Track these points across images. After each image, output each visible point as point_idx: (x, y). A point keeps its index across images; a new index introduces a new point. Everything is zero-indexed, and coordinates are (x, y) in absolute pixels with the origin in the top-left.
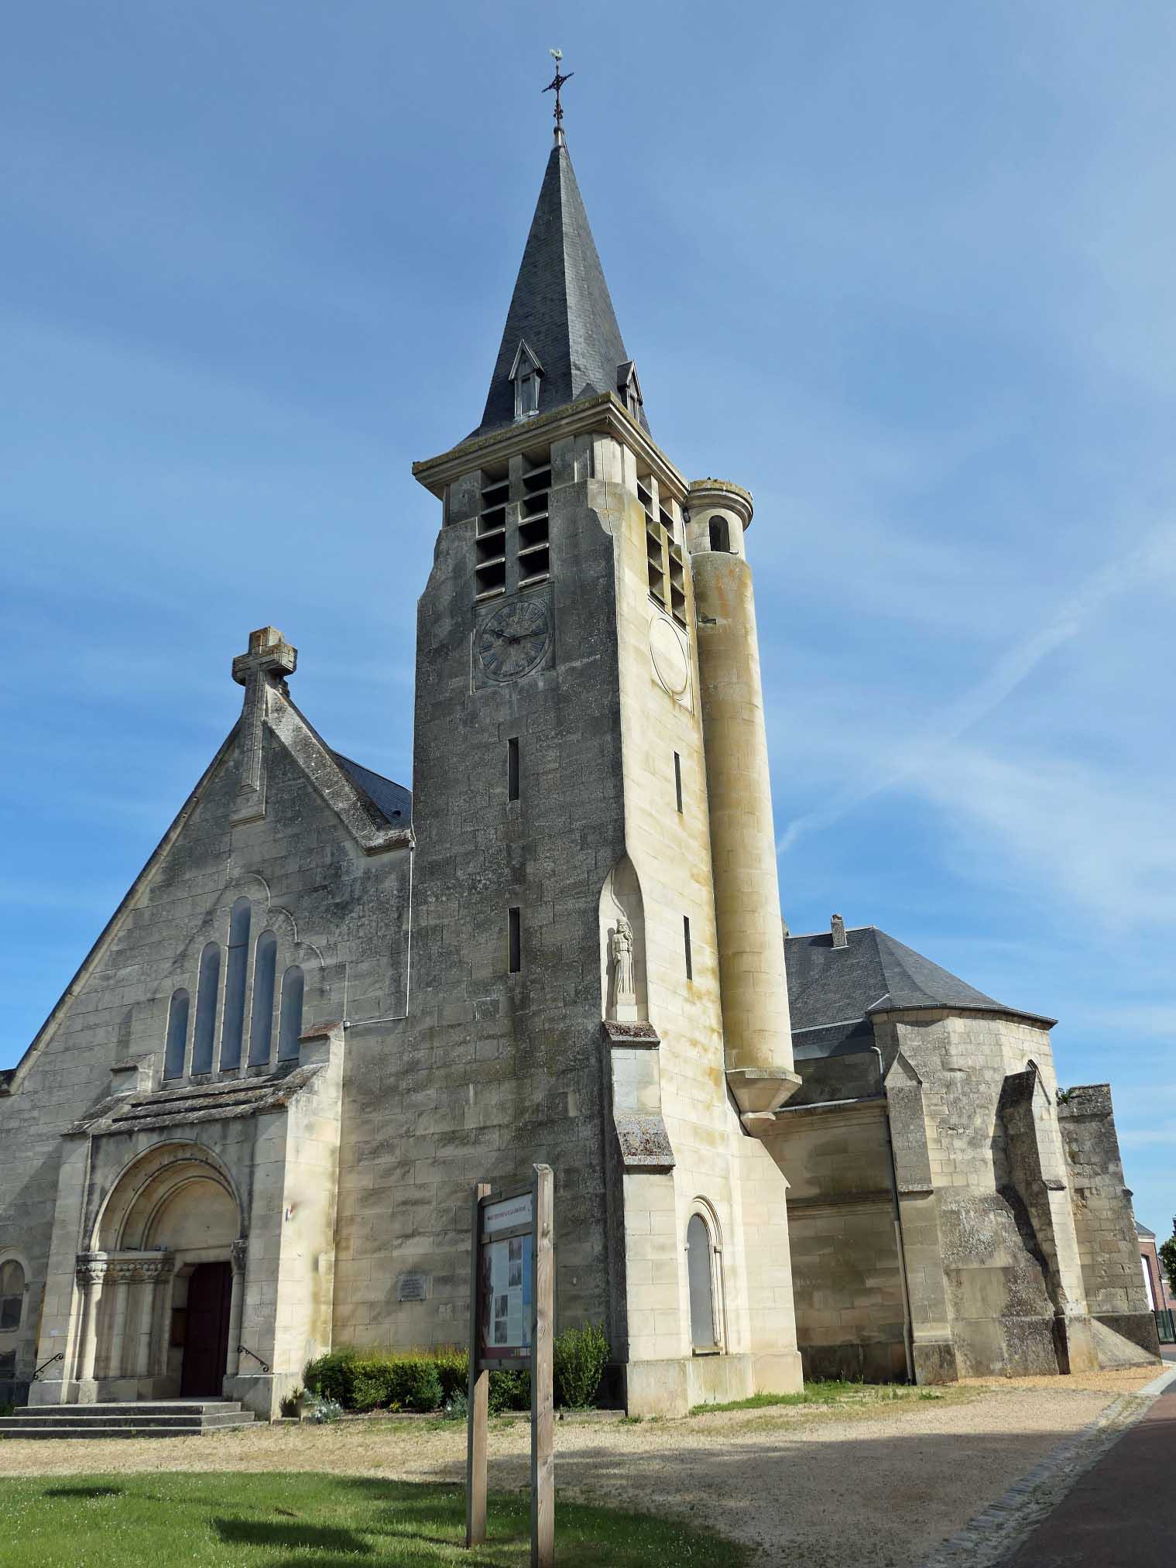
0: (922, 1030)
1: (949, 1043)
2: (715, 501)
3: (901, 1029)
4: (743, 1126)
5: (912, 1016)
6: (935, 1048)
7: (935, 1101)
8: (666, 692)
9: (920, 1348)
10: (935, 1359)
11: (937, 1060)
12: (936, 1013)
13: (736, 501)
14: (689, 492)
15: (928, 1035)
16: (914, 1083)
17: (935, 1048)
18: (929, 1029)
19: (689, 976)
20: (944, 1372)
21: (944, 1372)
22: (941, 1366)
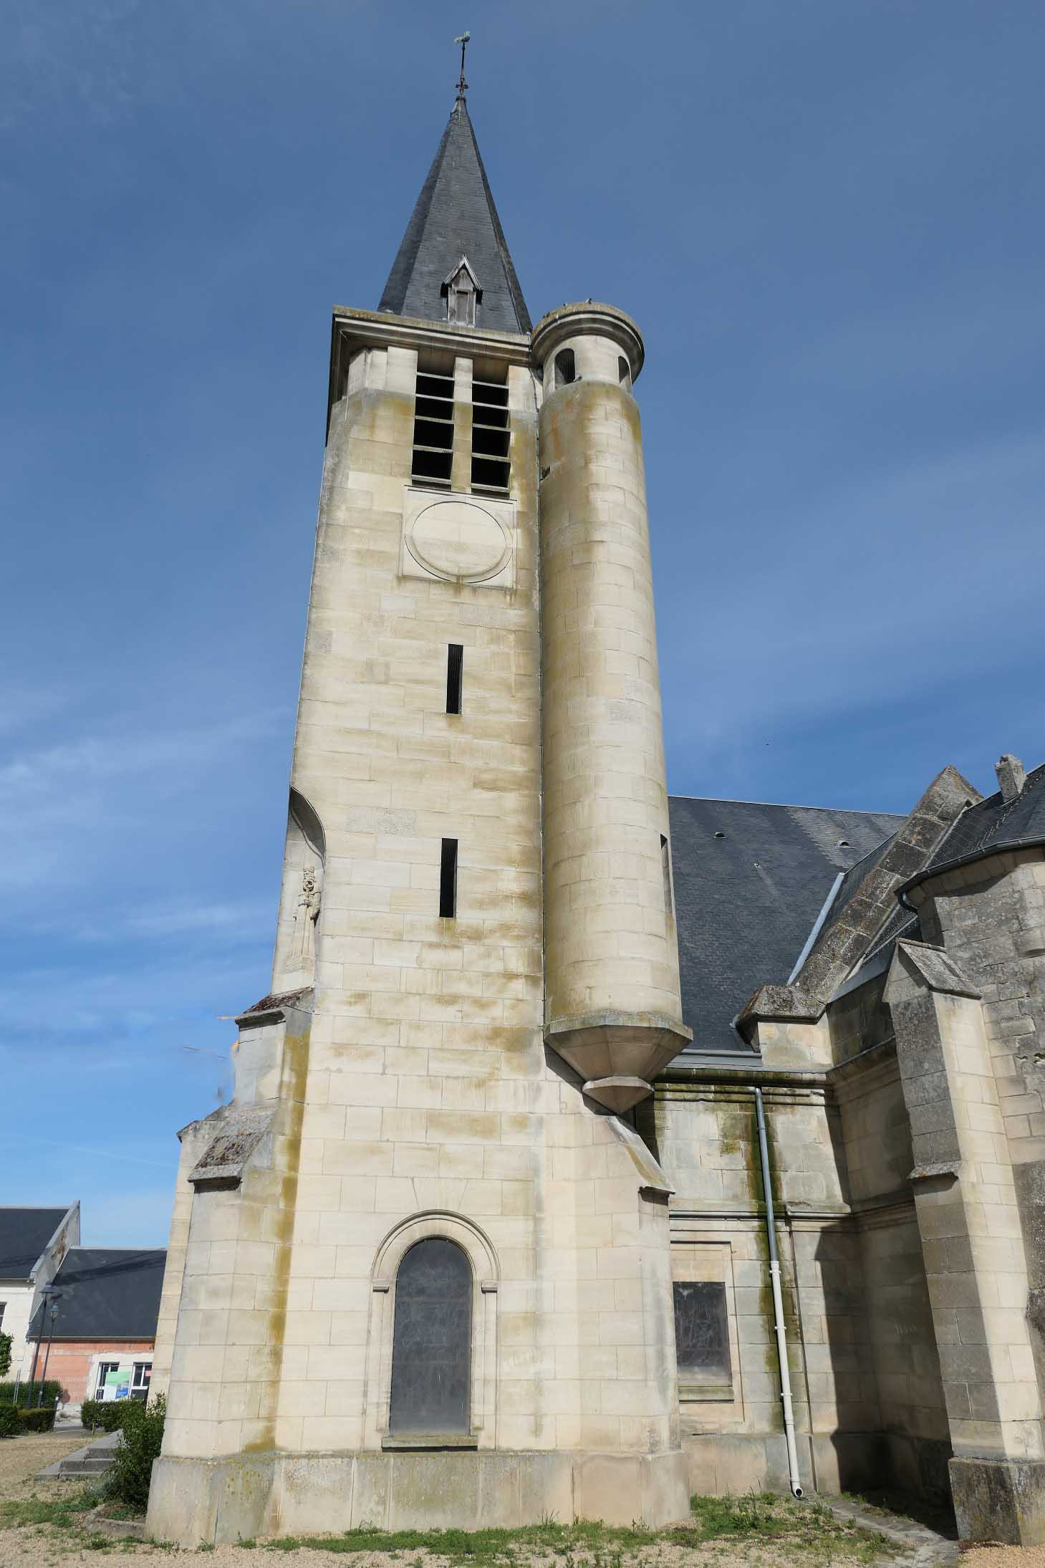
0: (977, 898)
1: (1024, 908)
2: (554, 336)
3: (943, 904)
4: (588, 1099)
5: (958, 878)
6: (1000, 923)
7: (1007, 1012)
8: (447, 583)
9: (962, 1468)
10: (982, 1491)
11: (1006, 942)
12: (993, 864)
13: (580, 321)
14: (530, 347)
15: (987, 904)
16: (924, 989)
17: (1000, 923)
18: (988, 894)
19: (447, 908)
20: (998, 1521)
21: (998, 1521)
22: (993, 1510)
